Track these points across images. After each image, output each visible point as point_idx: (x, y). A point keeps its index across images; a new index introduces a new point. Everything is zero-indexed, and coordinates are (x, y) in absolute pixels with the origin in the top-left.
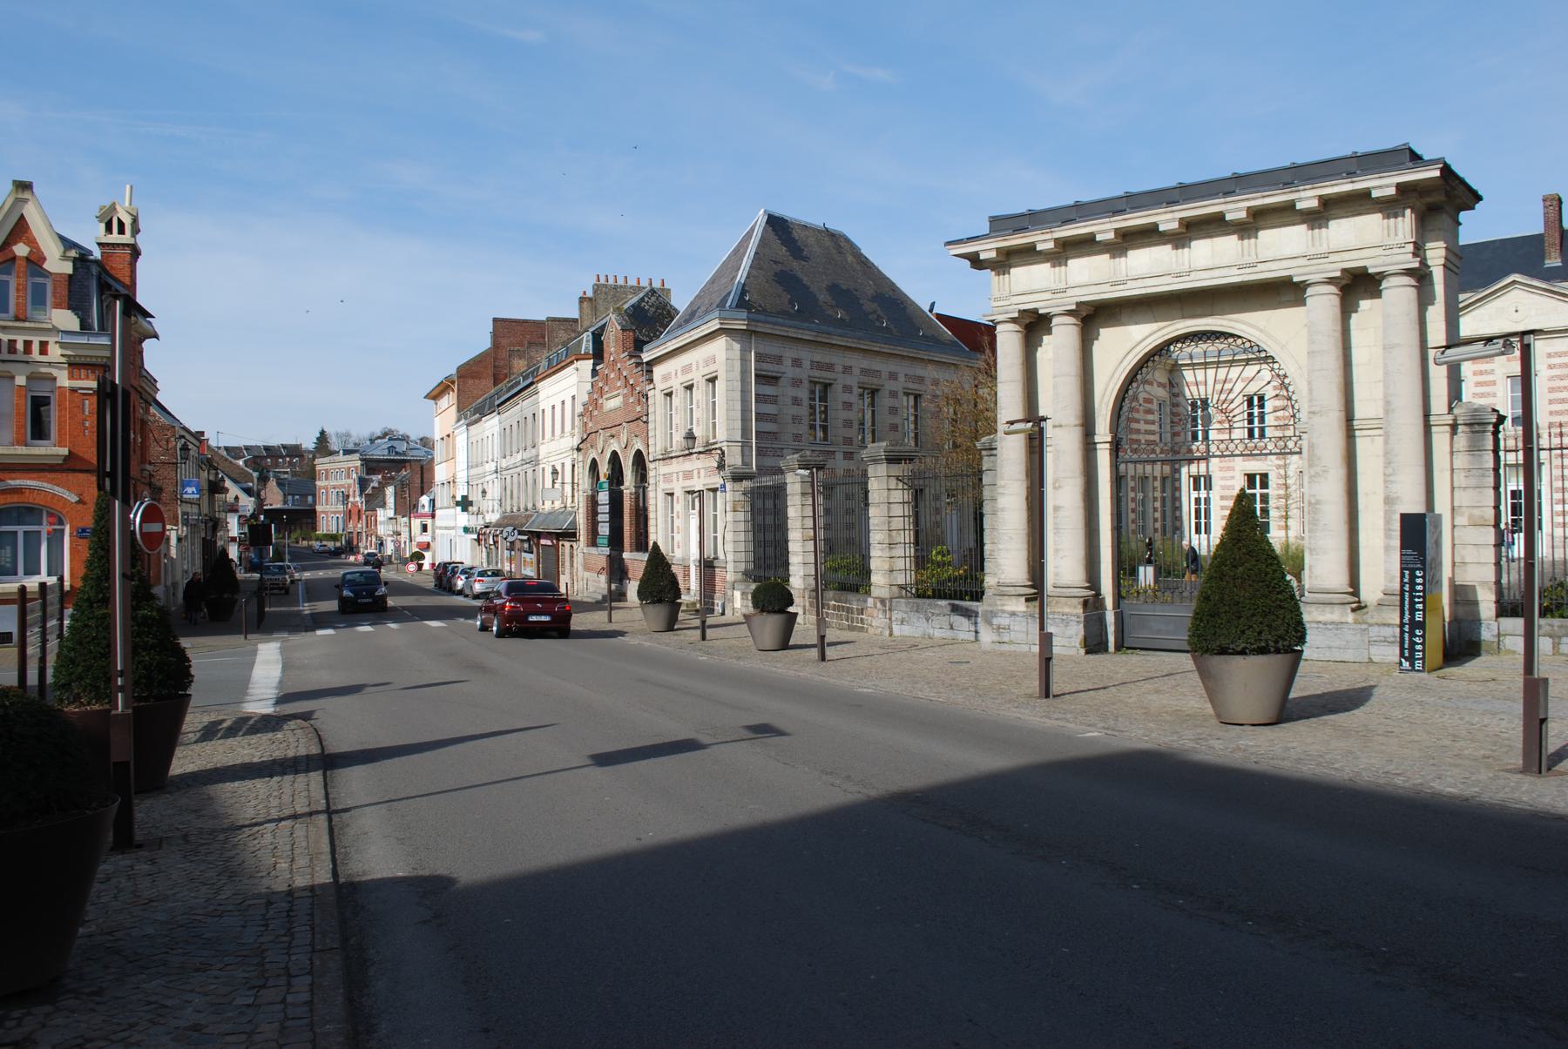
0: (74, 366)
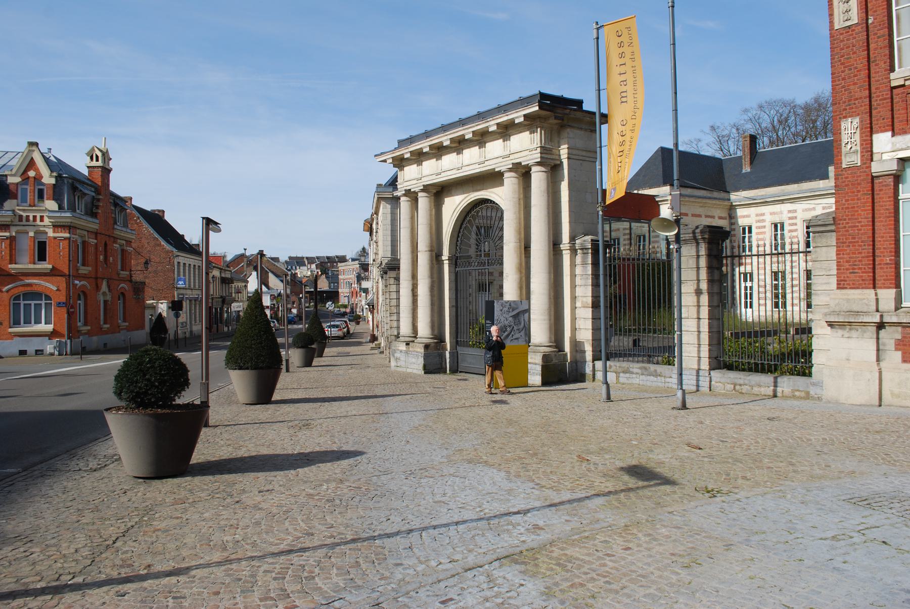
0: (56, 227)
